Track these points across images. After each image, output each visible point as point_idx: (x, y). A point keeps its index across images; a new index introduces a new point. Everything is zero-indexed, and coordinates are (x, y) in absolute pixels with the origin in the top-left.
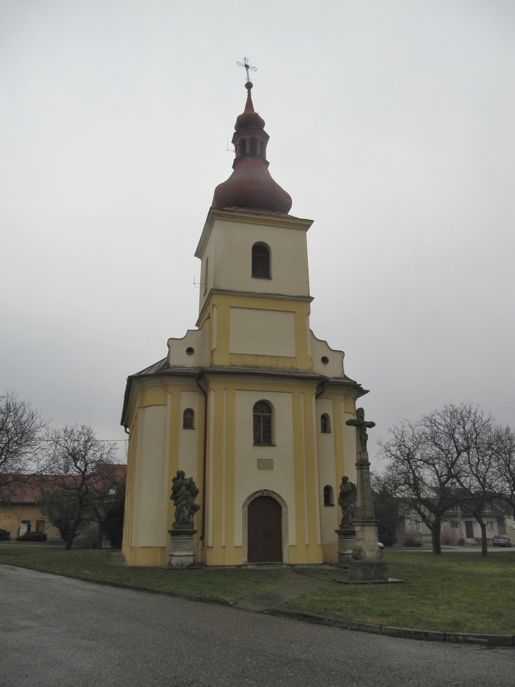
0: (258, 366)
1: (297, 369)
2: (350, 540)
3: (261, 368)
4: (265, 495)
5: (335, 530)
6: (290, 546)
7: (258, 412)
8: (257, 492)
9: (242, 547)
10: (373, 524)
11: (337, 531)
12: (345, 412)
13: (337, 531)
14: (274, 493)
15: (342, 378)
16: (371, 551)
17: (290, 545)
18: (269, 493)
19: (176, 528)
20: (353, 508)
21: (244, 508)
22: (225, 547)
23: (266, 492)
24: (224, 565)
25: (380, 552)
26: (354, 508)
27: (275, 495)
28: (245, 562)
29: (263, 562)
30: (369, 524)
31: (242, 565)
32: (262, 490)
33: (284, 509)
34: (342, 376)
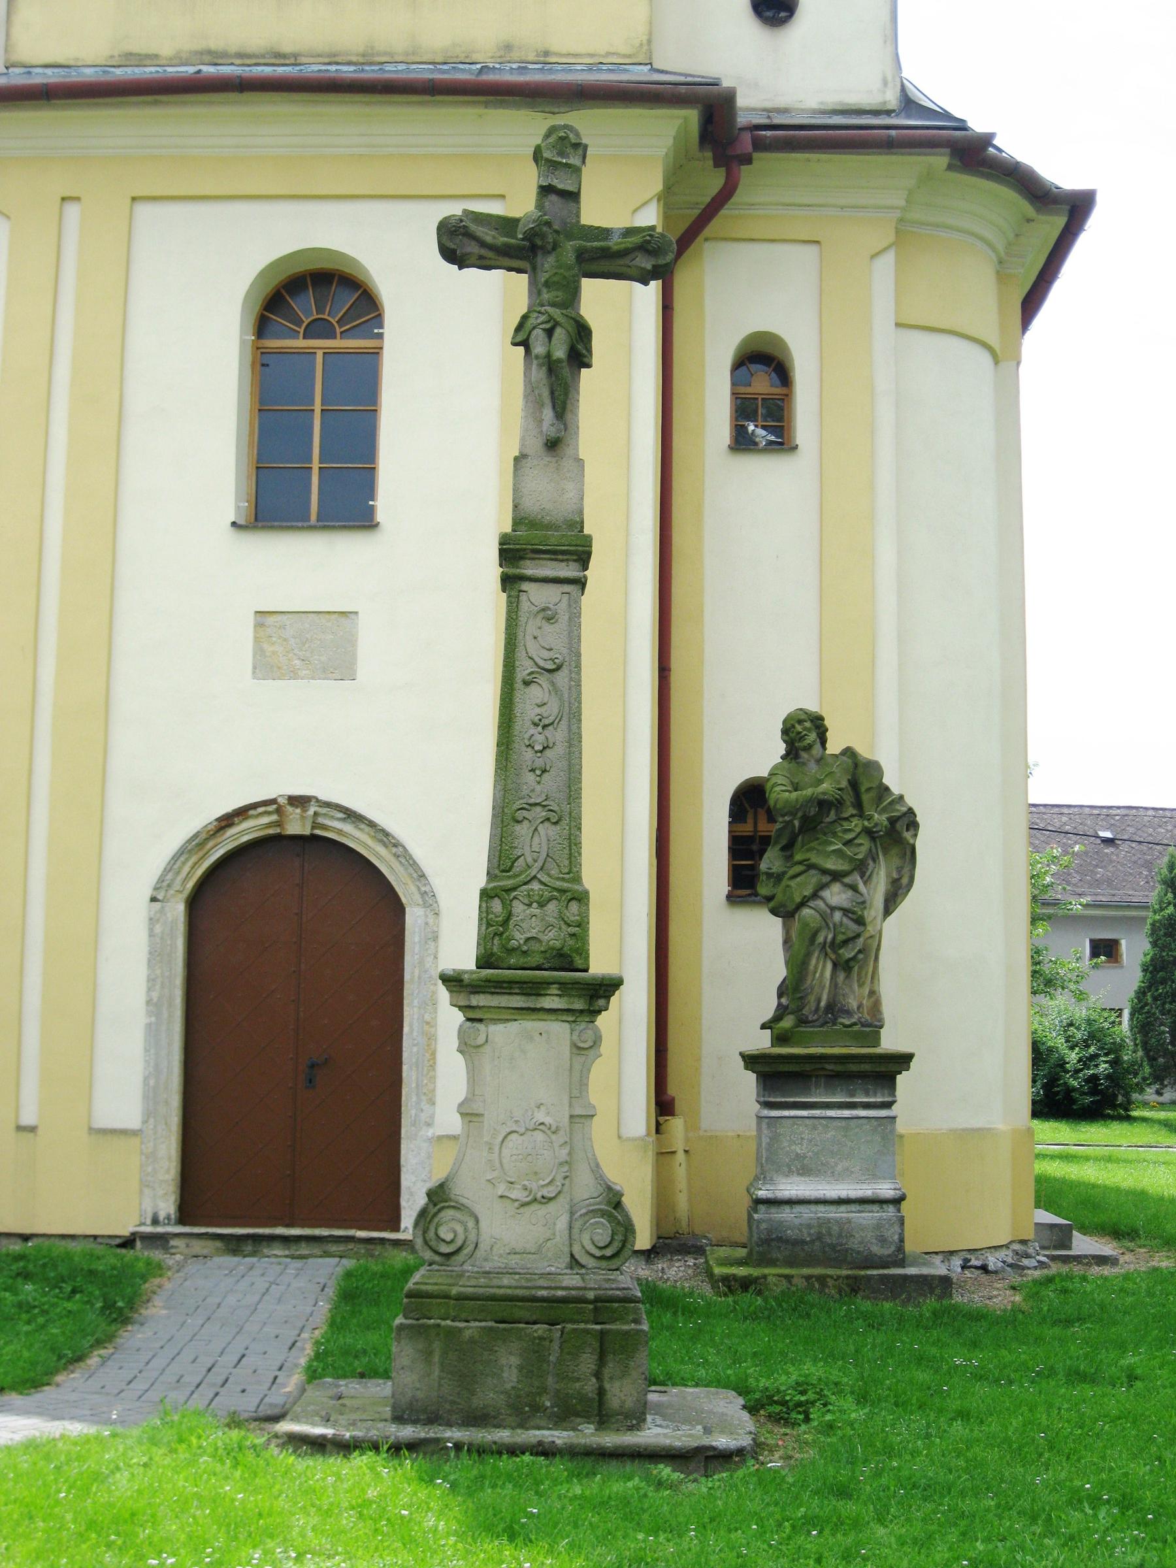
0: (287, 48)
1: (546, 53)
2: (804, 1113)
3: (304, 60)
4: (296, 826)
5: (743, 1049)
6: (440, 1138)
7: (294, 335)
8: (242, 813)
9: (134, 1133)
10: (551, 1002)
11: (751, 1061)
12: (898, 325)
13: (751, 1061)
14: (351, 815)
15: (890, 107)
16: (524, 1205)
17: (440, 1132)
18: (320, 820)
19: (780, 1039)
20: (838, 916)
21: (157, 905)
22: (32, 1129)
23: (298, 811)
24: (28, 1231)
25: (603, 1214)
26: (846, 911)
27: (357, 834)
28: (155, 1221)
29: (275, 1225)
30: (518, 1001)
31: (133, 1234)
32: (273, 801)
33: (414, 917)
34: (891, 98)
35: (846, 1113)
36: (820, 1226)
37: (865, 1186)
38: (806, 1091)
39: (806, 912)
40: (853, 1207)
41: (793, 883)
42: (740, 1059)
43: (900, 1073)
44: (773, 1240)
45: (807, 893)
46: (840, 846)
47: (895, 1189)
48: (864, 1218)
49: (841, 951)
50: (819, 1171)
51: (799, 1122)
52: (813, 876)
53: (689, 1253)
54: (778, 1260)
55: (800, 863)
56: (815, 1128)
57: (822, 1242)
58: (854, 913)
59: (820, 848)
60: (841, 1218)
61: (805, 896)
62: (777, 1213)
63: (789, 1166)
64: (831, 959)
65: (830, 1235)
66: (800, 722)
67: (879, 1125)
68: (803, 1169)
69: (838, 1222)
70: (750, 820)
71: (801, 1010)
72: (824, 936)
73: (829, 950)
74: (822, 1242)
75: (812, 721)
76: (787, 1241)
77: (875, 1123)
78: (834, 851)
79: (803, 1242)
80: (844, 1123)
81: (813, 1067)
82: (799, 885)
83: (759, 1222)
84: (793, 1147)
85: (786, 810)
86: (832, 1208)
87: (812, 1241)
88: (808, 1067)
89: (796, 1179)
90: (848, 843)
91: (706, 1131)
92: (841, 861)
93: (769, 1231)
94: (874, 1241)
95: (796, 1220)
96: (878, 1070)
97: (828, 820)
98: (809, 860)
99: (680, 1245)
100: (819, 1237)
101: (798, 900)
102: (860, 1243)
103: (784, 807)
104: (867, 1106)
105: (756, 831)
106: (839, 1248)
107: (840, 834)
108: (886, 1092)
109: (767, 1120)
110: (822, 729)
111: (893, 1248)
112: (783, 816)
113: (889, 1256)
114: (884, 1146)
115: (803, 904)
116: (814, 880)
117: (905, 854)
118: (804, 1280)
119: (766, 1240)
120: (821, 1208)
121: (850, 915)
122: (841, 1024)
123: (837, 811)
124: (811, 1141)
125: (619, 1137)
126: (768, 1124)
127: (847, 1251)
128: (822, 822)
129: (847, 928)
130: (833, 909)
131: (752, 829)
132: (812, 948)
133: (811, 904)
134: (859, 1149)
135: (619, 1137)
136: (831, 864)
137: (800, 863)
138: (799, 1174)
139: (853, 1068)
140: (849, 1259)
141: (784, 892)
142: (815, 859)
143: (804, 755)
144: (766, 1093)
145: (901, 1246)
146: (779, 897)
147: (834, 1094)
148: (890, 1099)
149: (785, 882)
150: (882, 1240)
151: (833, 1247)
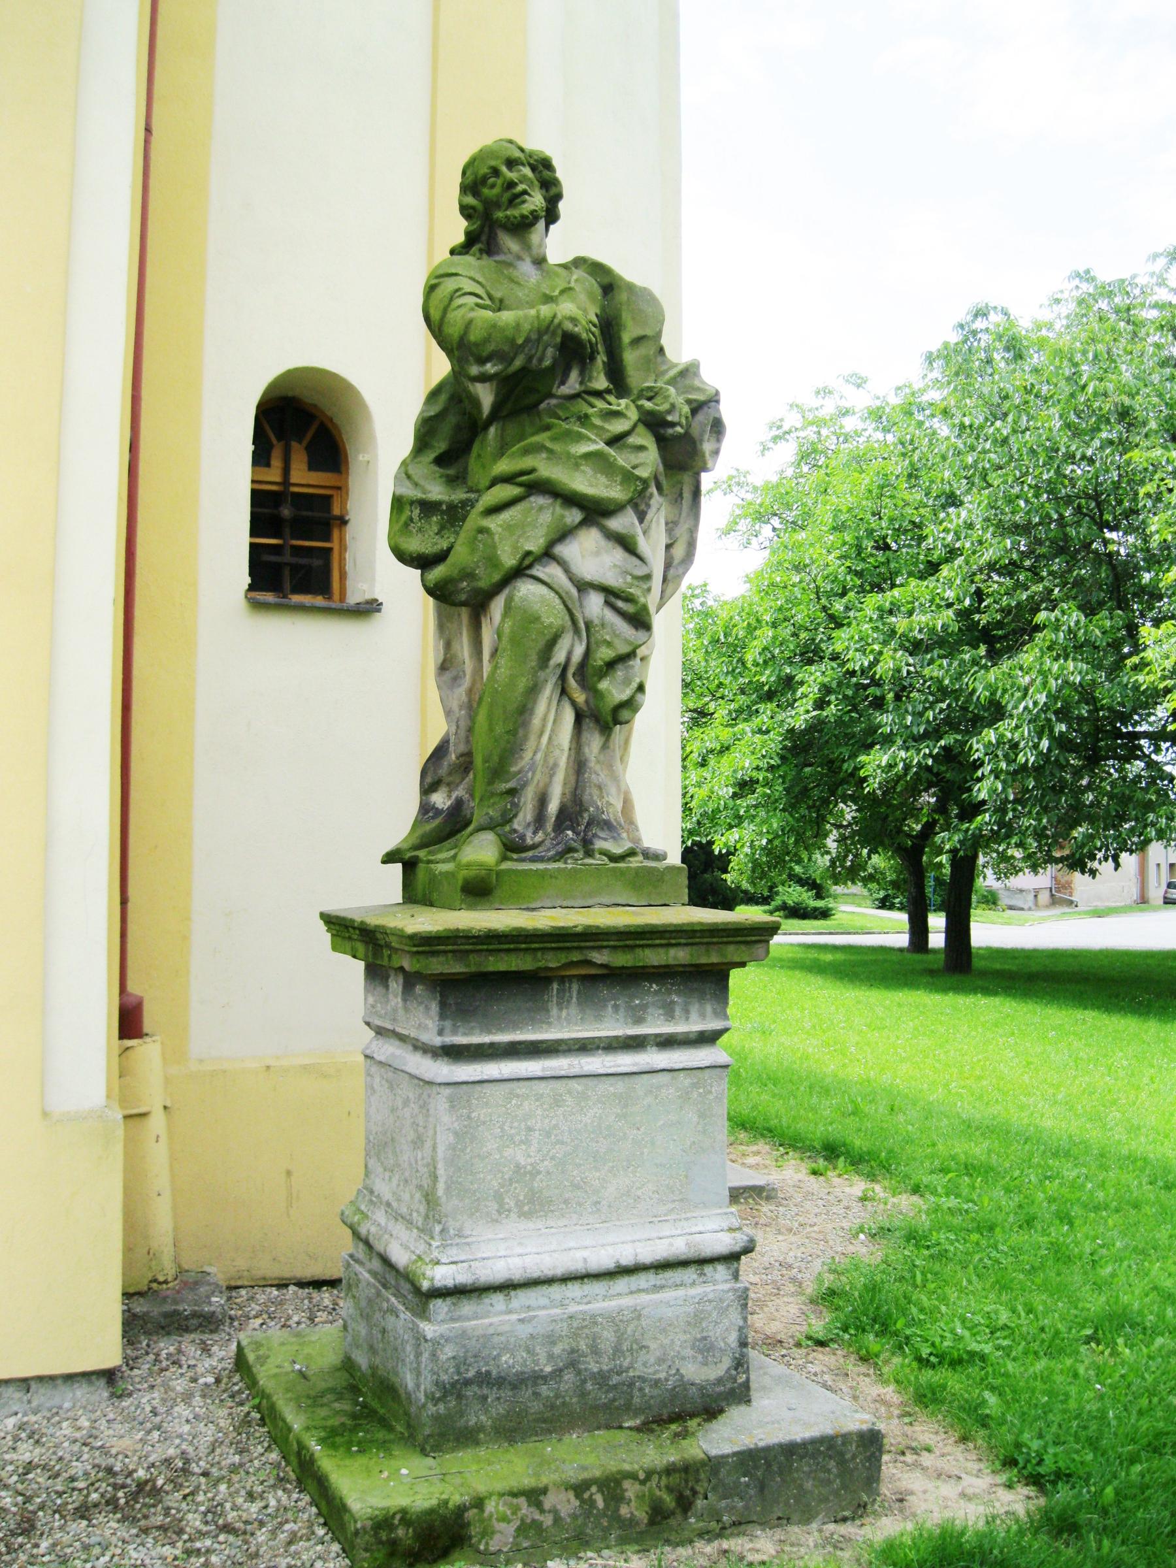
20: (595, 604)
26: (610, 594)
35: (626, 1061)
36: (575, 1335)
37: (667, 1230)
38: (538, 1013)
39: (525, 589)
40: (643, 1280)
41: (494, 523)
42: (322, 926)
43: (742, 964)
44: (467, 1383)
45: (535, 544)
46: (600, 446)
47: (731, 1230)
48: (668, 1304)
49: (604, 685)
50: (566, 1202)
51: (521, 1089)
52: (541, 508)
53: (187, 1330)
54: (480, 1428)
55: (508, 479)
56: (557, 1102)
57: (579, 1372)
58: (629, 599)
59: (557, 447)
60: (620, 1311)
61: (528, 553)
62: (476, 1317)
63: (499, 1198)
64: (573, 703)
65: (595, 1351)
66: (511, 163)
67: (695, 1086)
68: (531, 1201)
69: (614, 1320)
70: (276, 463)
71: (510, 821)
72: (570, 649)
73: (572, 683)
74: (579, 1372)
75: (534, 169)
76: (500, 1382)
77: (684, 1080)
78: (587, 456)
79: (538, 1378)
80: (620, 1085)
81: (563, 958)
82: (509, 528)
83: (436, 1343)
84: (508, 1152)
85: (491, 347)
86: (598, 1288)
87: (558, 1373)
88: (552, 961)
89: (513, 1225)
90: (616, 441)
91: (201, 1061)
92: (603, 479)
93: (460, 1363)
94: (688, 1352)
95: (520, 1327)
96: (704, 960)
97: (565, 390)
98: (532, 471)
99: (166, 1315)
100: (573, 1362)
101: (509, 560)
102: (660, 1361)
103: (487, 340)
104: (667, 1042)
105: (286, 482)
106: (615, 1379)
107: (597, 421)
108: (709, 1008)
109: (447, 1091)
110: (553, 191)
111: (727, 1363)
112: (482, 361)
113: (720, 1381)
114: (704, 1132)
115: (519, 572)
116: (546, 518)
117: (681, 495)
118: (571, 1495)
119: (453, 1385)
120: (574, 1290)
121: (620, 604)
122: (604, 853)
123: (582, 373)
124: (548, 1134)
125: (45, 1114)
126: (451, 1100)
127: (631, 1385)
128: (551, 395)
129: (615, 634)
130: (583, 586)
131: (278, 479)
132: (542, 675)
133: (538, 571)
134: (653, 1143)
135: (45, 1114)
136: (586, 483)
137: (508, 479)
138: (522, 1215)
139: (653, 957)
140: (636, 1400)
141: (473, 542)
142: (547, 470)
143: (510, 243)
144: (448, 1024)
145: (743, 1355)
146: (461, 555)
147: (599, 1018)
148: (714, 1025)
149: (474, 519)
150: (705, 1348)
151: (602, 1378)
